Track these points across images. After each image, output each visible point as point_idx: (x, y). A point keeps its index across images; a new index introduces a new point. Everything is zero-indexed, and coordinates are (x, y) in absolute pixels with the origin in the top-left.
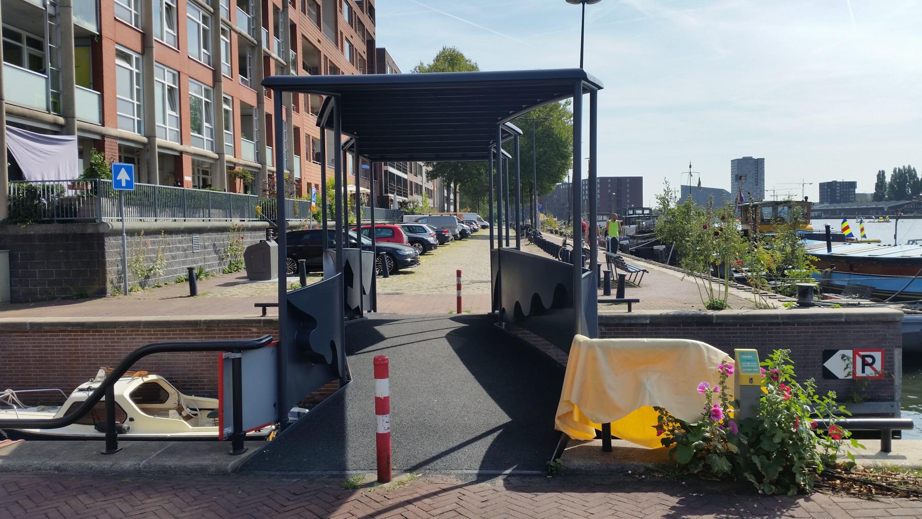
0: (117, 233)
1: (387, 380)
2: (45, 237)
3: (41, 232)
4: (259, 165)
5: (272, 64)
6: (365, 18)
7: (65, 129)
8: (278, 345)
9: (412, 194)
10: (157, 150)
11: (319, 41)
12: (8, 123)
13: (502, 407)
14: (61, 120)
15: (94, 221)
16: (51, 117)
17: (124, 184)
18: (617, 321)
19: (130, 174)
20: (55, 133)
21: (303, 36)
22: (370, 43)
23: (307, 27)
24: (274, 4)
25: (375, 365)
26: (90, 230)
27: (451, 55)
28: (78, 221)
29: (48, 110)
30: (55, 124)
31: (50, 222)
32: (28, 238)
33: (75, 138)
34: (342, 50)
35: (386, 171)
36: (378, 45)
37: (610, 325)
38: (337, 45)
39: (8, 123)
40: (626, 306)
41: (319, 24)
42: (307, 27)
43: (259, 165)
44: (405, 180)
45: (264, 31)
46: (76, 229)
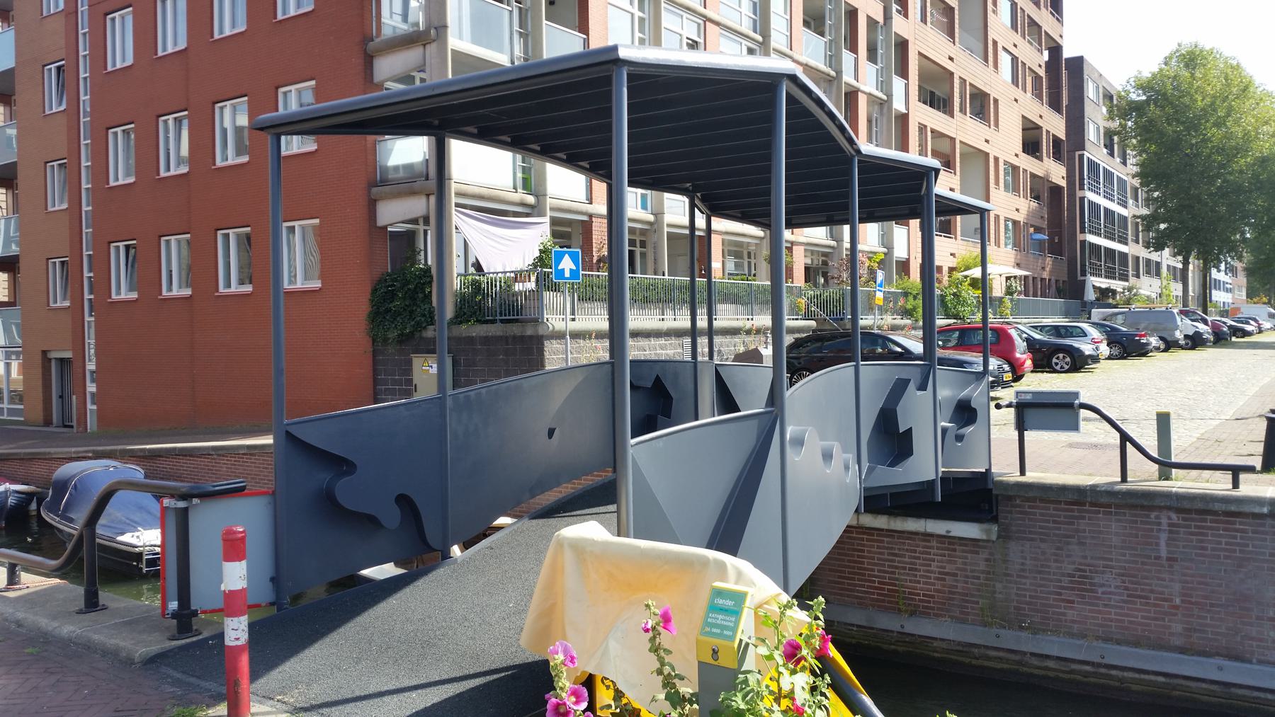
0: (560, 336)
1: (244, 563)
2: (487, 340)
3: (482, 334)
4: (833, 243)
5: (862, 101)
6: (1044, 18)
7: (534, 210)
8: (273, 493)
9: (1138, 276)
10: (666, 229)
11: (951, 59)
12: (457, 205)
13: (339, 626)
14: (531, 199)
15: (537, 321)
16: (520, 196)
17: (567, 274)
18: (1200, 506)
19: (576, 263)
20: (527, 215)
21: (920, 54)
22: (1055, 50)
23: (927, 41)
24: (868, 17)
25: (225, 540)
26: (529, 332)
27: (1191, 53)
28: (517, 321)
29: (515, 188)
30: (523, 204)
31: (493, 322)
32: (471, 340)
33: (547, 220)
34: (996, 66)
35: (1083, 242)
36: (1067, 53)
37: (1188, 511)
38: (986, 60)
39: (457, 205)
40: (1228, 476)
41: (951, 34)
42: (927, 41)
43: (833, 243)
44: (1124, 256)
45: (847, 56)
46: (515, 330)
